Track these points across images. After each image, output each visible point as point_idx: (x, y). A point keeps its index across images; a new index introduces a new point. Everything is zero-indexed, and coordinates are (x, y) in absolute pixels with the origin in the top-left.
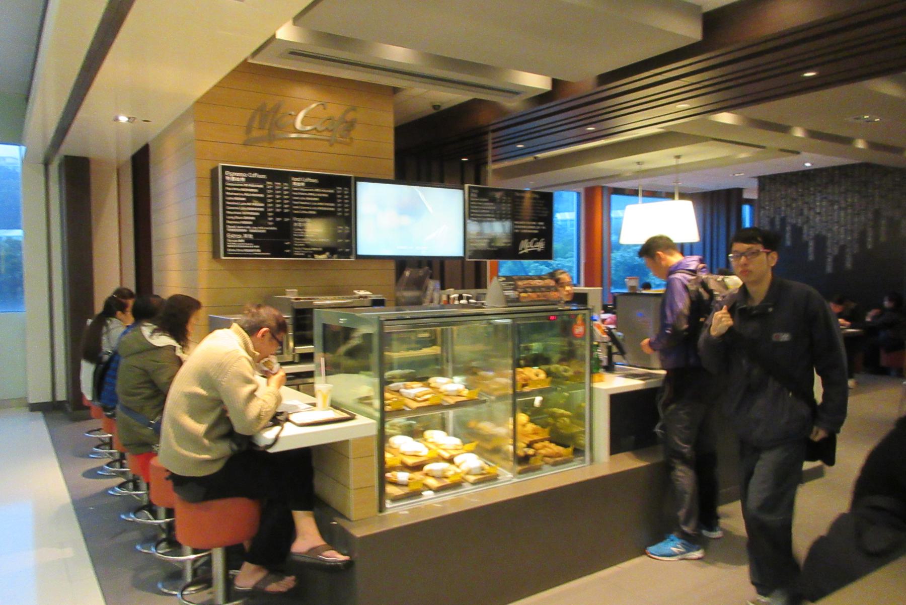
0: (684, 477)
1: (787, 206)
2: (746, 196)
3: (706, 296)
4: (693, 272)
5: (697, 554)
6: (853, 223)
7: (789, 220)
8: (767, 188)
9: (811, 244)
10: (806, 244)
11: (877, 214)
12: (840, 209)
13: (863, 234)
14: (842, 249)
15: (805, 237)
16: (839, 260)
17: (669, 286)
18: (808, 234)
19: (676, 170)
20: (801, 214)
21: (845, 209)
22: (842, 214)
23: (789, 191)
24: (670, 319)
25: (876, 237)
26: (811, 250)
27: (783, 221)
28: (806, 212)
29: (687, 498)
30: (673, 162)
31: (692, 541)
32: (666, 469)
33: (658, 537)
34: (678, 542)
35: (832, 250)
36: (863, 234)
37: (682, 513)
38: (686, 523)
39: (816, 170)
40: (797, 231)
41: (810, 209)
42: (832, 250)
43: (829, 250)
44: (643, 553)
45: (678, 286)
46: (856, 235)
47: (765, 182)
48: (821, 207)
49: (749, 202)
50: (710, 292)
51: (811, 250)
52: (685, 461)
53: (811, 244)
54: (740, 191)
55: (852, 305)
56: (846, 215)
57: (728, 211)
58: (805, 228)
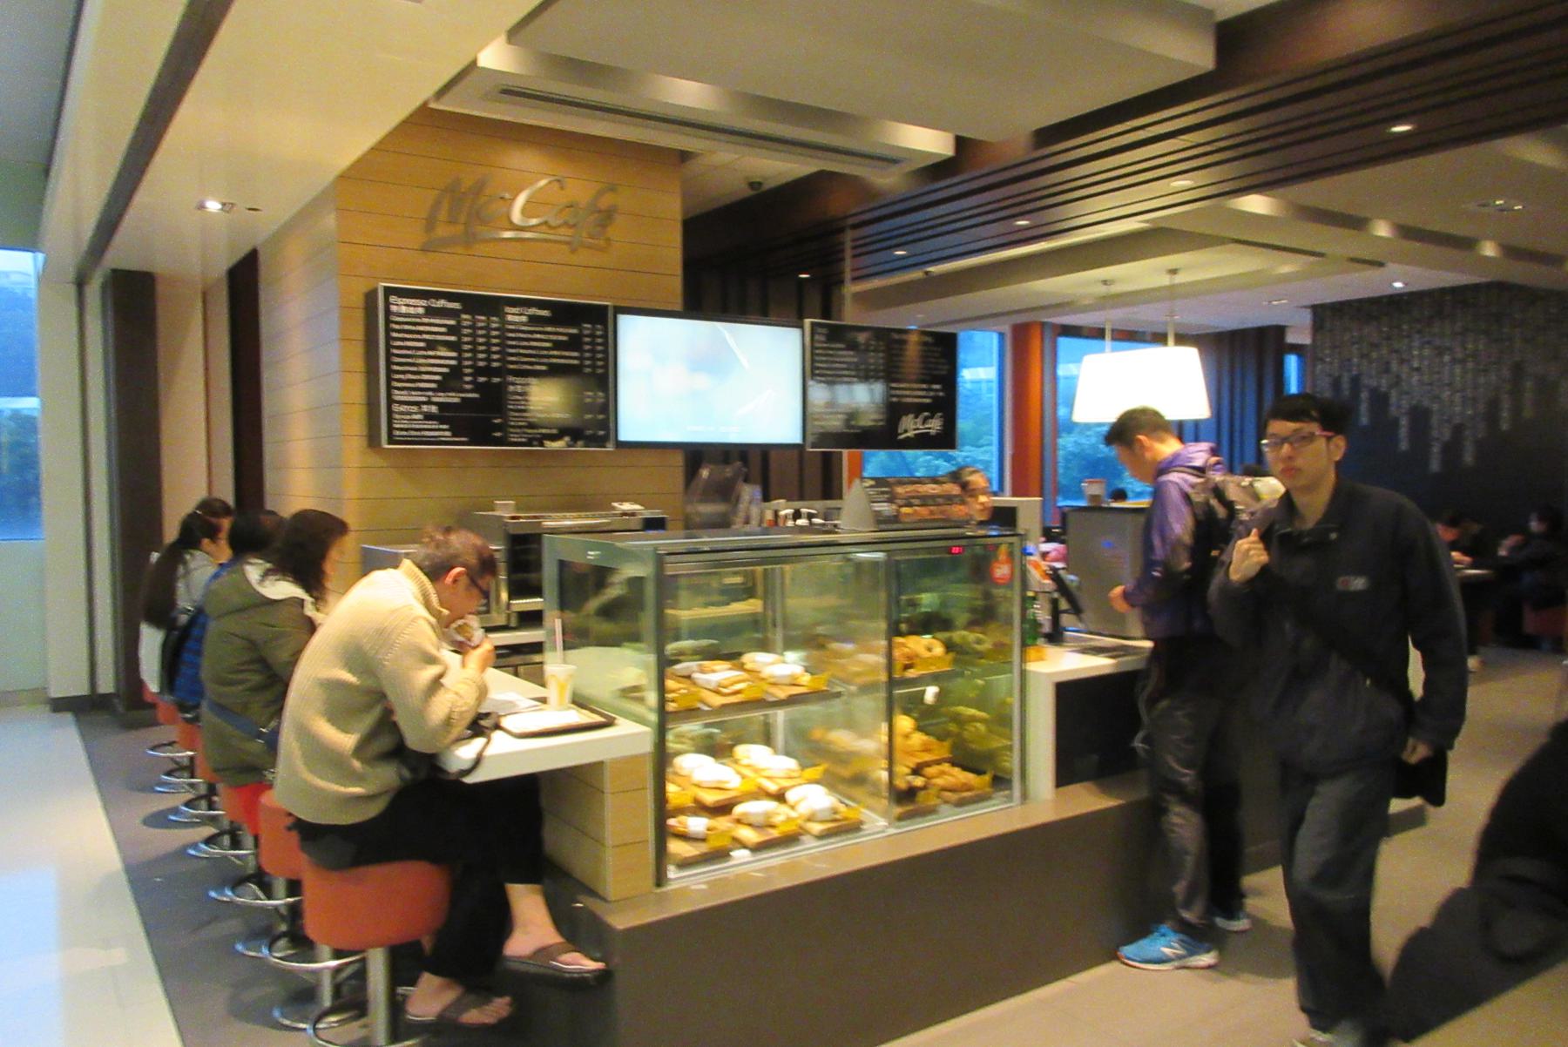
0: (1184, 825)
1: (1362, 356)
2: (1291, 338)
3: (1221, 512)
4: (1200, 471)
5: (1207, 959)
6: (1476, 387)
7: (1366, 381)
8: (1328, 325)
9: (1404, 422)
10: (1396, 422)
11: (1518, 370)
12: (1454, 361)
13: (1494, 405)
14: (1458, 430)
15: (1393, 411)
16: (1452, 449)
17: (1158, 494)
18: (1399, 406)
19: (1170, 294)
20: (1387, 370)
21: (1463, 361)
22: (1458, 370)
23: (1366, 331)
24: (1159, 553)
25: (1516, 410)
26: (1403, 432)
27: (1356, 382)
28: (1394, 366)
29: (1189, 861)
30: (1166, 280)
31: (1198, 936)
32: (1153, 812)
33: (1140, 930)
34: (1173, 938)
35: (1440, 433)
36: (1494, 405)
37: (1180, 888)
38: (1187, 905)
39: (1411, 294)
40: (1380, 401)
41: (1402, 362)
42: (1440, 433)
43: (1435, 433)
44: (1113, 956)
45: (1174, 495)
46: (1481, 407)
47: (1323, 315)
48: (1421, 358)
49: (1297, 349)
50: (1229, 505)
51: (1403, 432)
52: (1186, 798)
53: (1404, 422)
54: (1280, 330)
55: (1475, 528)
56: (1465, 372)
57: (1260, 366)
58: (1394, 394)
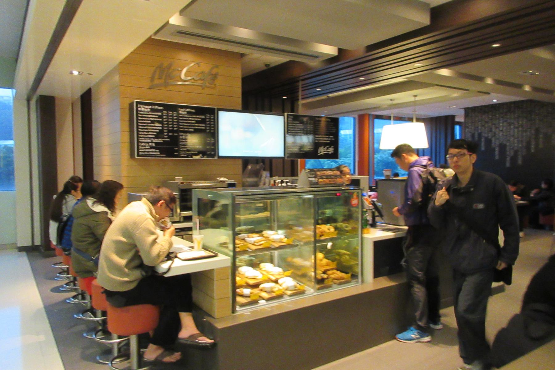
0: (419, 292)
1: (482, 126)
2: (457, 120)
3: (432, 181)
4: (425, 166)
5: (427, 339)
6: (522, 137)
7: (483, 135)
8: (470, 115)
9: (497, 149)
10: (494, 149)
11: (537, 131)
12: (515, 128)
13: (529, 143)
14: (516, 152)
15: (493, 145)
16: (514, 159)
17: (410, 175)
18: (495, 143)
19: (414, 104)
20: (491, 131)
21: (518, 128)
22: (516, 131)
23: (483, 117)
24: (410, 195)
25: (537, 145)
26: (497, 153)
27: (480, 135)
28: (494, 129)
29: (421, 304)
30: (413, 99)
31: (424, 331)
32: (408, 287)
33: (403, 329)
34: (415, 331)
35: (510, 153)
36: (529, 143)
37: (418, 314)
38: (420, 320)
39: (500, 104)
40: (488, 142)
41: (496, 128)
42: (510, 153)
43: (508, 153)
44: (394, 338)
45: (416, 175)
46: (524, 144)
47: (468, 111)
48: (503, 126)
49: (459, 123)
50: (435, 178)
51: (497, 153)
52: (420, 282)
53: (497, 149)
54: (453, 117)
55: (522, 187)
56: (518, 131)
57: (446, 129)
58: (493, 139)
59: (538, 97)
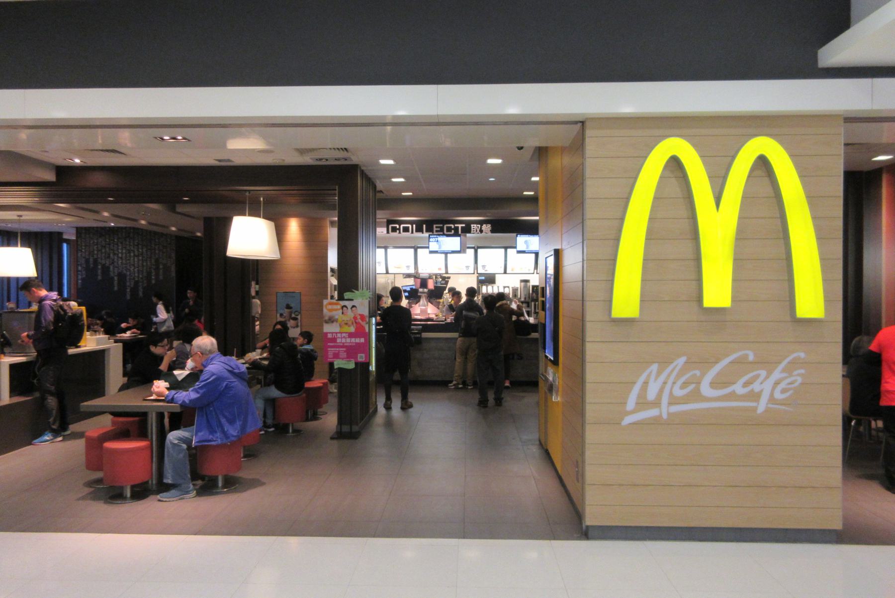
0: (52, 402)
1: (98, 251)
2: (65, 237)
3: (62, 313)
4: (55, 301)
5: (60, 439)
6: (143, 266)
7: (99, 260)
8: (83, 235)
9: (116, 278)
10: (113, 278)
11: (157, 261)
12: (135, 256)
13: (149, 274)
14: (136, 283)
15: (112, 274)
16: (134, 291)
17: (41, 308)
18: (113, 272)
19: (19, 221)
20: (109, 257)
21: (138, 256)
22: (136, 259)
23: (100, 240)
24: (44, 324)
25: (157, 275)
26: (116, 282)
27: (96, 261)
28: (111, 255)
29: (54, 412)
30: (16, 218)
31: (56, 433)
32: (43, 399)
33: (37, 434)
34: (50, 435)
35: (130, 284)
36: (149, 274)
37: (51, 420)
38: (53, 424)
39: (118, 228)
40: (106, 270)
41: (114, 254)
42: (130, 284)
43: (128, 284)
44: (30, 444)
45: (48, 308)
46: (145, 274)
47: (80, 231)
48: (122, 253)
49: (67, 241)
50: (64, 311)
51: (116, 282)
52: (52, 394)
53: (116, 278)
54: (60, 234)
55: (142, 320)
56: (139, 260)
57: (51, 248)
58: (111, 267)
59: (151, 228)
